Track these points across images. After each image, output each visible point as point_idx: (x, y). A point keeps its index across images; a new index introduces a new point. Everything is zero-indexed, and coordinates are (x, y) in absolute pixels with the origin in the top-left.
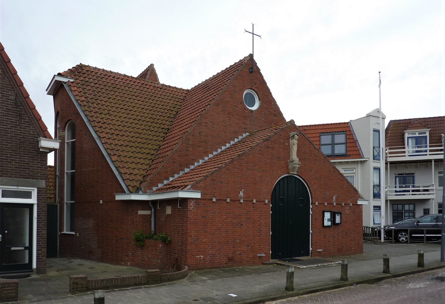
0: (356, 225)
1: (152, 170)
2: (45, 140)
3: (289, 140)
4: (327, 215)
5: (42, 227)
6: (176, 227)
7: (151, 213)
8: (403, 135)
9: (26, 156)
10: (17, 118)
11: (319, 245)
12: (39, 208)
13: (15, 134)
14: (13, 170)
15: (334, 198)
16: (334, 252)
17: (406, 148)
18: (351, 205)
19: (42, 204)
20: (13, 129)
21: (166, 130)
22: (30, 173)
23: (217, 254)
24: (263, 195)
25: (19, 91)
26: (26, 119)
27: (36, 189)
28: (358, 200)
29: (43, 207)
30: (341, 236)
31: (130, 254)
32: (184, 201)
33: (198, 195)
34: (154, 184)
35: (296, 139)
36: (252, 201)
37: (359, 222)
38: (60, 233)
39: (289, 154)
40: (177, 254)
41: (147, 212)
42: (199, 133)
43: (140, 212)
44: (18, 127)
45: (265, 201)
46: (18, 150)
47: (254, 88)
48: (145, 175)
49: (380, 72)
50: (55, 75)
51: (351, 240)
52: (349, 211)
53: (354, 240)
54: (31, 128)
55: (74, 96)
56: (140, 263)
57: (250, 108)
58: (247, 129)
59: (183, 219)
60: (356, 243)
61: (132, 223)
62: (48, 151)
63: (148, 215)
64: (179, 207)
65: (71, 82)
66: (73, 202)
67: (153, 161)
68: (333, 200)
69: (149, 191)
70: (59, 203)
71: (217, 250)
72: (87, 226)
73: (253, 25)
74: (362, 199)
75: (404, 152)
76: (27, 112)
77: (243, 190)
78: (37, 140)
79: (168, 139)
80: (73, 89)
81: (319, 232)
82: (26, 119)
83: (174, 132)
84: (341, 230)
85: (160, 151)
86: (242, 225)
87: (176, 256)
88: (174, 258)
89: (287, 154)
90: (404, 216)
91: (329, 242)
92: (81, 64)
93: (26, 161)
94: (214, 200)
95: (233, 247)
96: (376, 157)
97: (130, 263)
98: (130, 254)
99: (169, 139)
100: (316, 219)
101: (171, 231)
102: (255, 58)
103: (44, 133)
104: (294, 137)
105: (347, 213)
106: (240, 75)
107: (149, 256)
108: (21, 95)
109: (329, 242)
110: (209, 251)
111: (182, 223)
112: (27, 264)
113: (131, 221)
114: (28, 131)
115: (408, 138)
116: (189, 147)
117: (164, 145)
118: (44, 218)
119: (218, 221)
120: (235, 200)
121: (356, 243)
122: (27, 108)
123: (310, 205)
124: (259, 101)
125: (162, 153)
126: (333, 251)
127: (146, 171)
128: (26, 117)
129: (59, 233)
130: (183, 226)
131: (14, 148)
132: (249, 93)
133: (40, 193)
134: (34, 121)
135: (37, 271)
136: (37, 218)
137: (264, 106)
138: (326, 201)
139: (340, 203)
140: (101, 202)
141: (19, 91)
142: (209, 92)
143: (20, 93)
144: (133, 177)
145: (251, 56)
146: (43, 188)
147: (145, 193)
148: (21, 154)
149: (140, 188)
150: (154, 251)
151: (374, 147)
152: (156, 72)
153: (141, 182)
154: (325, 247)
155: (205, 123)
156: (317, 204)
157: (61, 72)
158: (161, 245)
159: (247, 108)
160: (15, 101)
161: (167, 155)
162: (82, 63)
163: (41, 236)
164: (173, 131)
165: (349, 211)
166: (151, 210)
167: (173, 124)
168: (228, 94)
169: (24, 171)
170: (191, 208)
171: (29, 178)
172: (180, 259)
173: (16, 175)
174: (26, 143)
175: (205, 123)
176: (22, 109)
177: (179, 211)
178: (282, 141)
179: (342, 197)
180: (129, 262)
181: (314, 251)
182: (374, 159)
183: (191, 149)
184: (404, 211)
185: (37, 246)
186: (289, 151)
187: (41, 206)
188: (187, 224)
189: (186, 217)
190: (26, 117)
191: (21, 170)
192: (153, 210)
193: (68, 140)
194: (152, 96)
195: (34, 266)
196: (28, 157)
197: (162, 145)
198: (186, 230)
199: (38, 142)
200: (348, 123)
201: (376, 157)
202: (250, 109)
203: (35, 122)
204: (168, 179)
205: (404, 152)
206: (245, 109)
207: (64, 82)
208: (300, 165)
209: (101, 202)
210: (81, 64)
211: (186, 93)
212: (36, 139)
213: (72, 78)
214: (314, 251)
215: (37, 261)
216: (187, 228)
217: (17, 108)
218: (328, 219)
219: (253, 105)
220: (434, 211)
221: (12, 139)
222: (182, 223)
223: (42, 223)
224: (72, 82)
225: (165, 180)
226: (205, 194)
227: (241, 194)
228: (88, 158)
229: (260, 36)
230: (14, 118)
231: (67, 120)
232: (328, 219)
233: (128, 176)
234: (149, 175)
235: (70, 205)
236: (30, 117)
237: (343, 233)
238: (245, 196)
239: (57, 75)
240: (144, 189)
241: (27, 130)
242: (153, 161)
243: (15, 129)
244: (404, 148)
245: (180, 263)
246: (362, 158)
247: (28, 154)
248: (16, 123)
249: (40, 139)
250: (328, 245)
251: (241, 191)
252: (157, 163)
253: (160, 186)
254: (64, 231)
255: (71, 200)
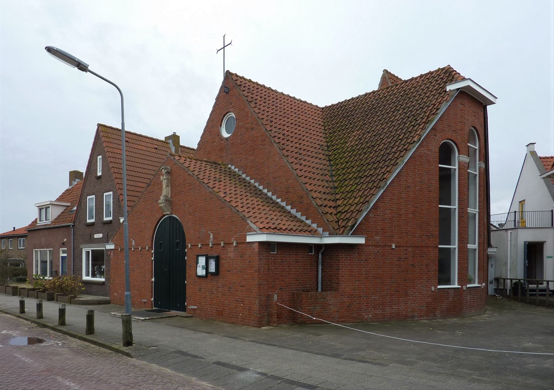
0: (246, 276)
11: (193, 301)
16: (211, 314)
30: (222, 292)
37: (252, 271)
51: (237, 301)
52: (235, 255)
53: (242, 301)
60: (246, 307)
73: (218, 51)
74: (255, 233)
81: (194, 283)
84: (221, 283)
91: (205, 298)
100: (190, 266)
105: (230, 257)
109: (205, 298)
121: (246, 307)
126: (211, 312)
137: (240, 124)
165: (235, 255)
179: (223, 233)
194: (281, 125)
208: (165, 203)
218: (202, 266)
220: (62, 248)
232: (202, 266)
237: (223, 288)
238: (136, 244)
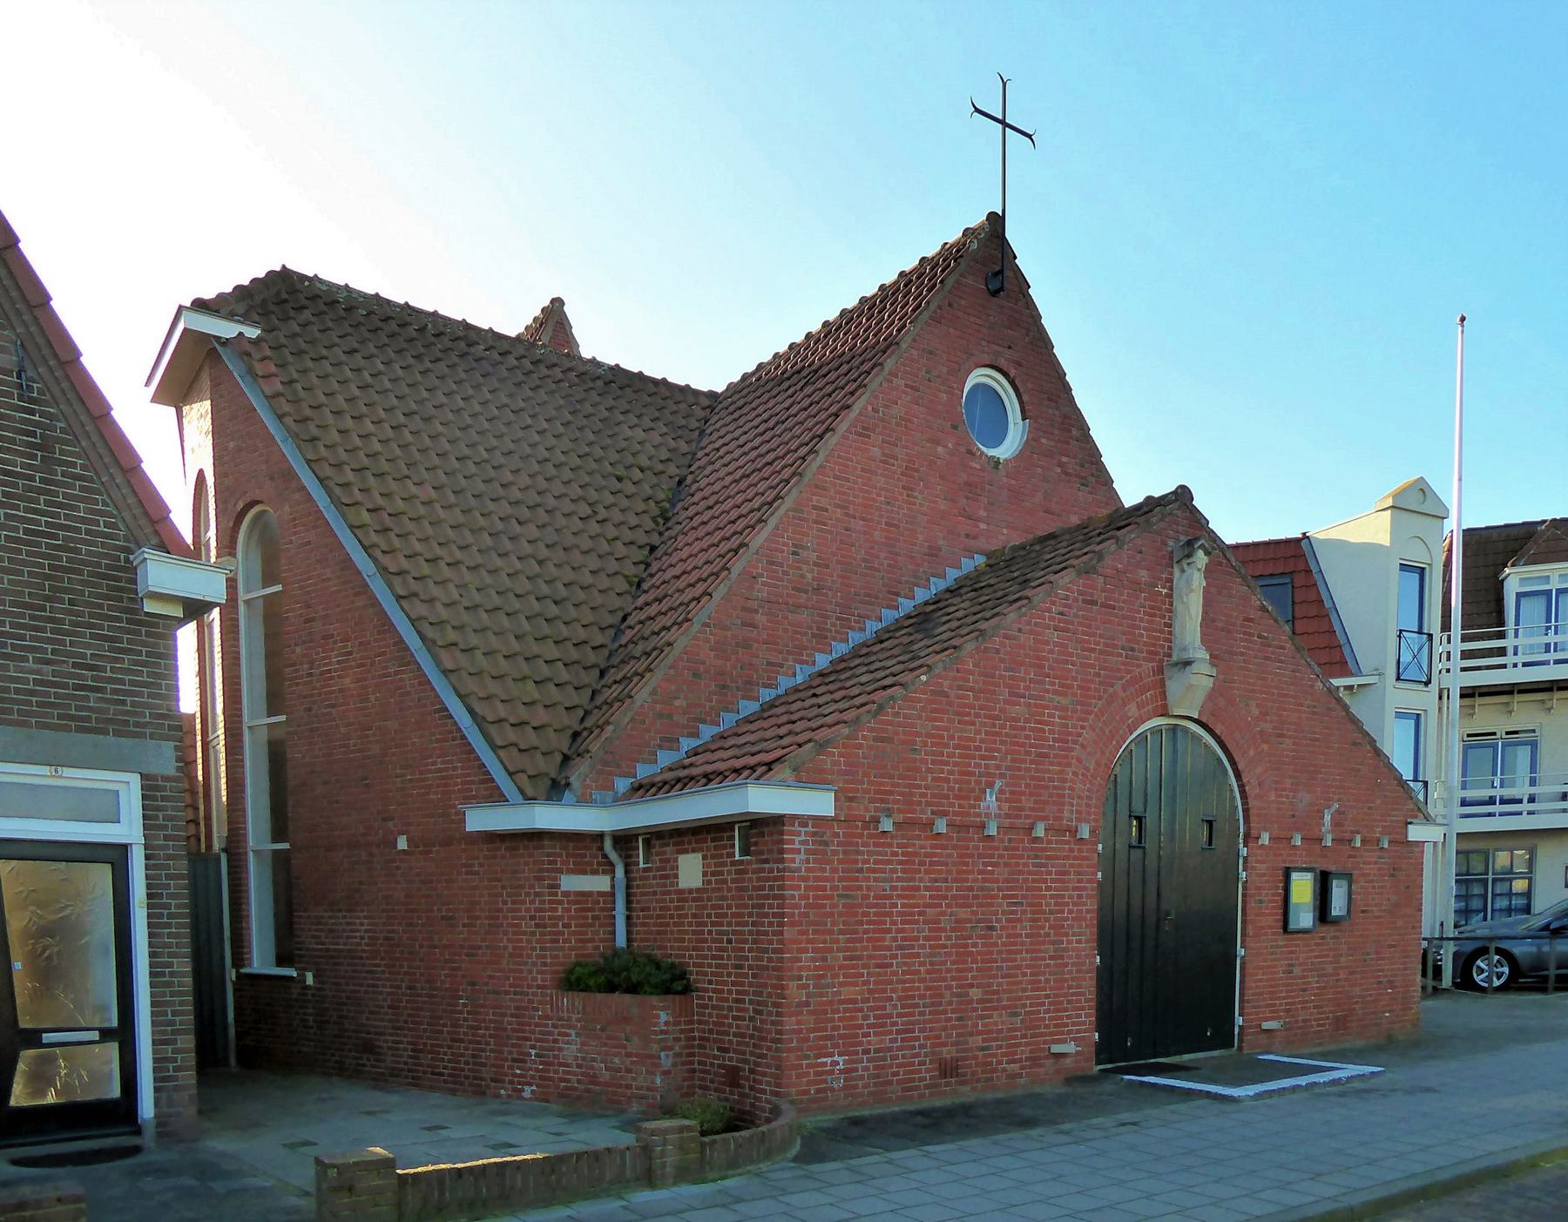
1: (605, 708)
2: (162, 559)
3: (1171, 574)
4: (1303, 888)
5: (169, 946)
6: (729, 941)
7: (613, 886)
8: (1499, 587)
9: (83, 635)
10: (34, 457)
12: (152, 862)
13: (26, 531)
14: (32, 693)
15: (1327, 818)
17: (1511, 633)
18: (1386, 846)
19: (166, 847)
20: (17, 508)
21: (646, 552)
22: (106, 711)
23: (899, 1049)
24: (1072, 805)
25: (33, 329)
26: (73, 465)
27: (135, 780)
28: (1411, 823)
29: (169, 857)
31: (533, 1052)
32: (762, 827)
33: (819, 803)
34: (618, 766)
35: (1199, 570)
36: (1031, 828)
38: (237, 972)
39: (1170, 633)
40: (735, 1051)
41: (600, 883)
42: (794, 553)
43: (572, 883)
44: (42, 498)
45: (1077, 831)
46: (48, 604)
47: (1002, 362)
48: (578, 728)
49: (1463, 319)
50: (181, 308)
53: (1391, 982)
54: (100, 507)
55: (266, 397)
56: (576, 1089)
57: (991, 452)
58: (975, 538)
59: (762, 906)
61: (537, 926)
62: (178, 612)
63: (601, 894)
64: (737, 858)
65: (250, 341)
66: (285, 846)
67: (602, 673)
68: (1420, 813)
69: (600, 795)
70: (225, 850)
71: (898, 1032)
72: (344, 944)
75: (1502, 652)
76: (77, 430)
77: (998, 784)
78: (127, 560)
79: (659, 582)
80: (259, 369)
82: (73, 465)
83: (684, 553)
85: (628, 631)
86: (992, 928)
87: (731, 1059)
88: (719, 1066)
89: (1162, 632)
90: (1494, 895)
92: (284, 266)
93: (83, 656)
94: (887, 825)
95: (959, 1019)
96: (1405, 669)
97: (534, 1088)
98: (533, 1052)
99: (664, 582)
101: (706, 957)
102: (1014, 235)
103: (156, 533)
104: (1189, 561)
106: (950, 305)
107: (616, 1060)
108: (46, 351)
110: (867, 1035)
111: (754, 924)
112: (113, 1102)
113: (532, 918)
114: (83, 520)
115: (1519, 596)
116: (756, 611)
117: (641, 609)
118: (178, 906)
119: (900, 914)
120: (968, 827)
122: (75, 411)
123: (1241, 846)
124: (1023, 420)
125: (643, 638)
127: (581, 713)
128: (71, 454)
129: (232, 974)
130: (758, 933)
131: (29, 593)
132: (985, 386)
133: (155, 798)
134: (111, 475)
135: (160, 1129)
136: (149, 906)
138: (1298, 829)
139: (1347, 836)
140: (402, 843)
141: (33, 329)
142: (819, 384)
143: (40, 340)
144: (532, 738)
145: (996, 221)
146: (166, 778)
147: (584, 800)
148: (62, 622)
149: (563, 782)
150: (635, 1039)
151: (1401, 631)
152: (573, 331)
153: (566, 759)
154: (1288, 1011)
155: (815, 508)
156: (1265, 839)
157: (209, 294)
158: (663, 1016)
159: (978, 449)
160: (19, 377)
161: (669, 644)
162: (292, 266)
163: (169, 984)
164: (676, 549)
166: (610, 868)
167: (669, 525)
168: (906, 386)
169: (100, 617)
170: (797, 861)
171: (105, 732)
172: (752, 1071)
173: (46, 715)
174: (80, 572)
175: (815, 508)
176: (51, 417)
177: (739, 872)
178: (1143, 575)
180: (530, 1084)
181: (1251, 1027)
182: (1398, 679)
183: (764, 619)
184: (1490, 877)
185: (154, 1024)
186: (1170, 618)
187: (161, 853)
188: (781, 924)
189: (775, 897)
190: (71, 454)
191: (68, 696)
192: (620, 872)
193: (248, 591)
195: (147, 1107)
196: (93, 636)
197: (636, 608)
198: (775, 951)
199: (131, 572)
200: (1298, 541)
201: (1405, 669)
202: (990, 454)
203: (114, 480)
204: (671, 743)
205: (1502, 652)
206: (970, 452)
207: (218, 338)
209: (402, 843)
210: (284, 266)
211: (708, 407)
212: (122, 558)
213: (254, 323)
214: (1251, 1027)
215: (157, 1090)
216: (781, 942)
217: (32, 412)
219: (998, 439)
221: (19, 551)
222: (754, 924)
223: (168, 925)
224: (256, 342)
225: (661, 747)
226: (851, 799)
227: (988, 798)
228: (339, 662)
229: (1029, 136)
230: (21, 454)
231: (241, 505)
233: (512, 735)
234: (598, 727)
235: (269, 860)
236: (93, 456)
239: (189, 305)
240: (585, 787)
241: (82, 514)
242: (602, 673)
243: (27, 510)
244: (1502, 635)
245: (752, 1088)
246: (1351, 674)
247: (91, 626)
248: (32, 478)
249: (141, 558)
250: (1300, 1002)
251: (991, 785)
252: (624, 678)
253: (643, 772)
254: (250, 965)
255: (275, 840)
